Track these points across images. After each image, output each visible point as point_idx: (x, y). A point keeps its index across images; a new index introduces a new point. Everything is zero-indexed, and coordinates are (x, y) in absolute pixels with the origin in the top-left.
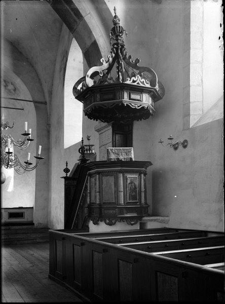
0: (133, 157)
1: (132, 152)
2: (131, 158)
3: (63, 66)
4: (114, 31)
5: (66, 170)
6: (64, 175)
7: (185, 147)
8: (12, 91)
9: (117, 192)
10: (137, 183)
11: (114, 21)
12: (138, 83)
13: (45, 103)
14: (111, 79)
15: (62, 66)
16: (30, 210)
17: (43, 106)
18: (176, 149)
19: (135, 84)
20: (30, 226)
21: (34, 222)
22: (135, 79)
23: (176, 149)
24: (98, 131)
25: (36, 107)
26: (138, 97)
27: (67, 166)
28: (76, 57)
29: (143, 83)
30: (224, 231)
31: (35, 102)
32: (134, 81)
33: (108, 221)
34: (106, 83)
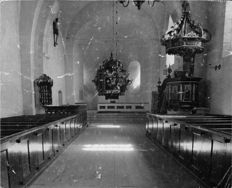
5: (159, 82)
12: (192, 36)
19: (190, 37)
22: (190, 34)
29: (194, 35)
32: (189, 35)
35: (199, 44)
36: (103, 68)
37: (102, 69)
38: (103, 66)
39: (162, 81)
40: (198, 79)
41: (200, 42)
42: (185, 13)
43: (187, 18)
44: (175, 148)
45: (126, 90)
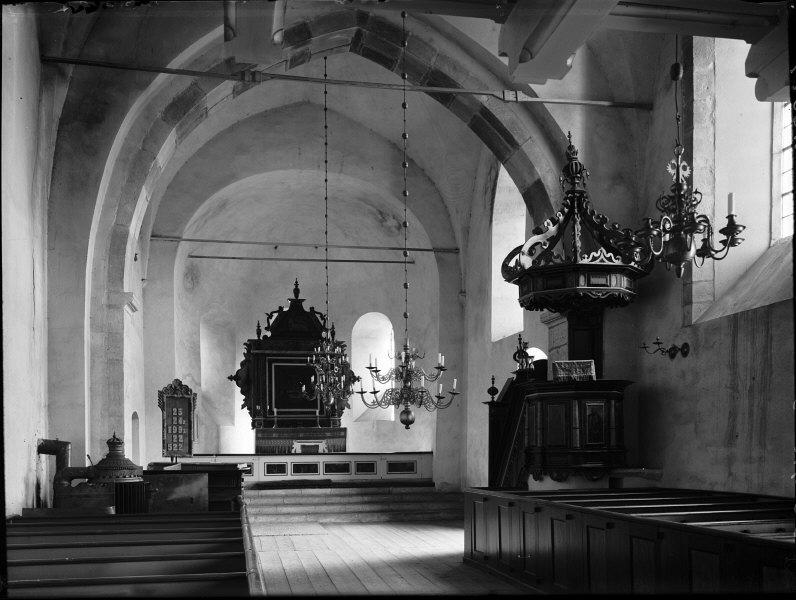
0: (594, 374)
1: (593, 367)
2: (591, 377)
3: (490, 185)
4: (569, 168)
5: (493, 391)
6: (489, 398)
7: (685, 354)
8: (394, 229)
9: (570, 428)
10: (603, 414)
11: (568, 155)
12: (602, 261)
13: (456, 251)
14: (558, 256)
15: (489, 185)
16: (429, 456)
17: (450, 257)
18: (672, 356)
19: (597, 262)
20: (426, 489)
21: (434, 481)
22: (596, 255)
23: (672, 356)
24: (546, 322)
25: (439, 260)
26: (602, 281)
27: (493, 383)
28: (508, 190)
29: (610, 259)
30: (793, 496)
31: (436, 250)
32: (594, 259)
33: (555, 475)
34: (551, 263)
35: (619, 284)
36: (269, 334)
37: (265, 337)
38: (266, 329)
39: (500, 386)
40: (620, 385)
41: (625, 279)
42: (573, 191)
43: (580, 206)
44: (576, 49)
45: (346, 410)
